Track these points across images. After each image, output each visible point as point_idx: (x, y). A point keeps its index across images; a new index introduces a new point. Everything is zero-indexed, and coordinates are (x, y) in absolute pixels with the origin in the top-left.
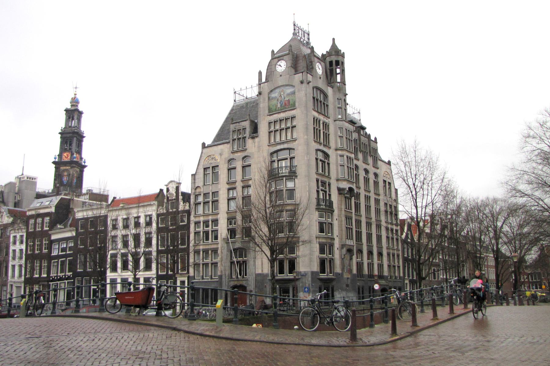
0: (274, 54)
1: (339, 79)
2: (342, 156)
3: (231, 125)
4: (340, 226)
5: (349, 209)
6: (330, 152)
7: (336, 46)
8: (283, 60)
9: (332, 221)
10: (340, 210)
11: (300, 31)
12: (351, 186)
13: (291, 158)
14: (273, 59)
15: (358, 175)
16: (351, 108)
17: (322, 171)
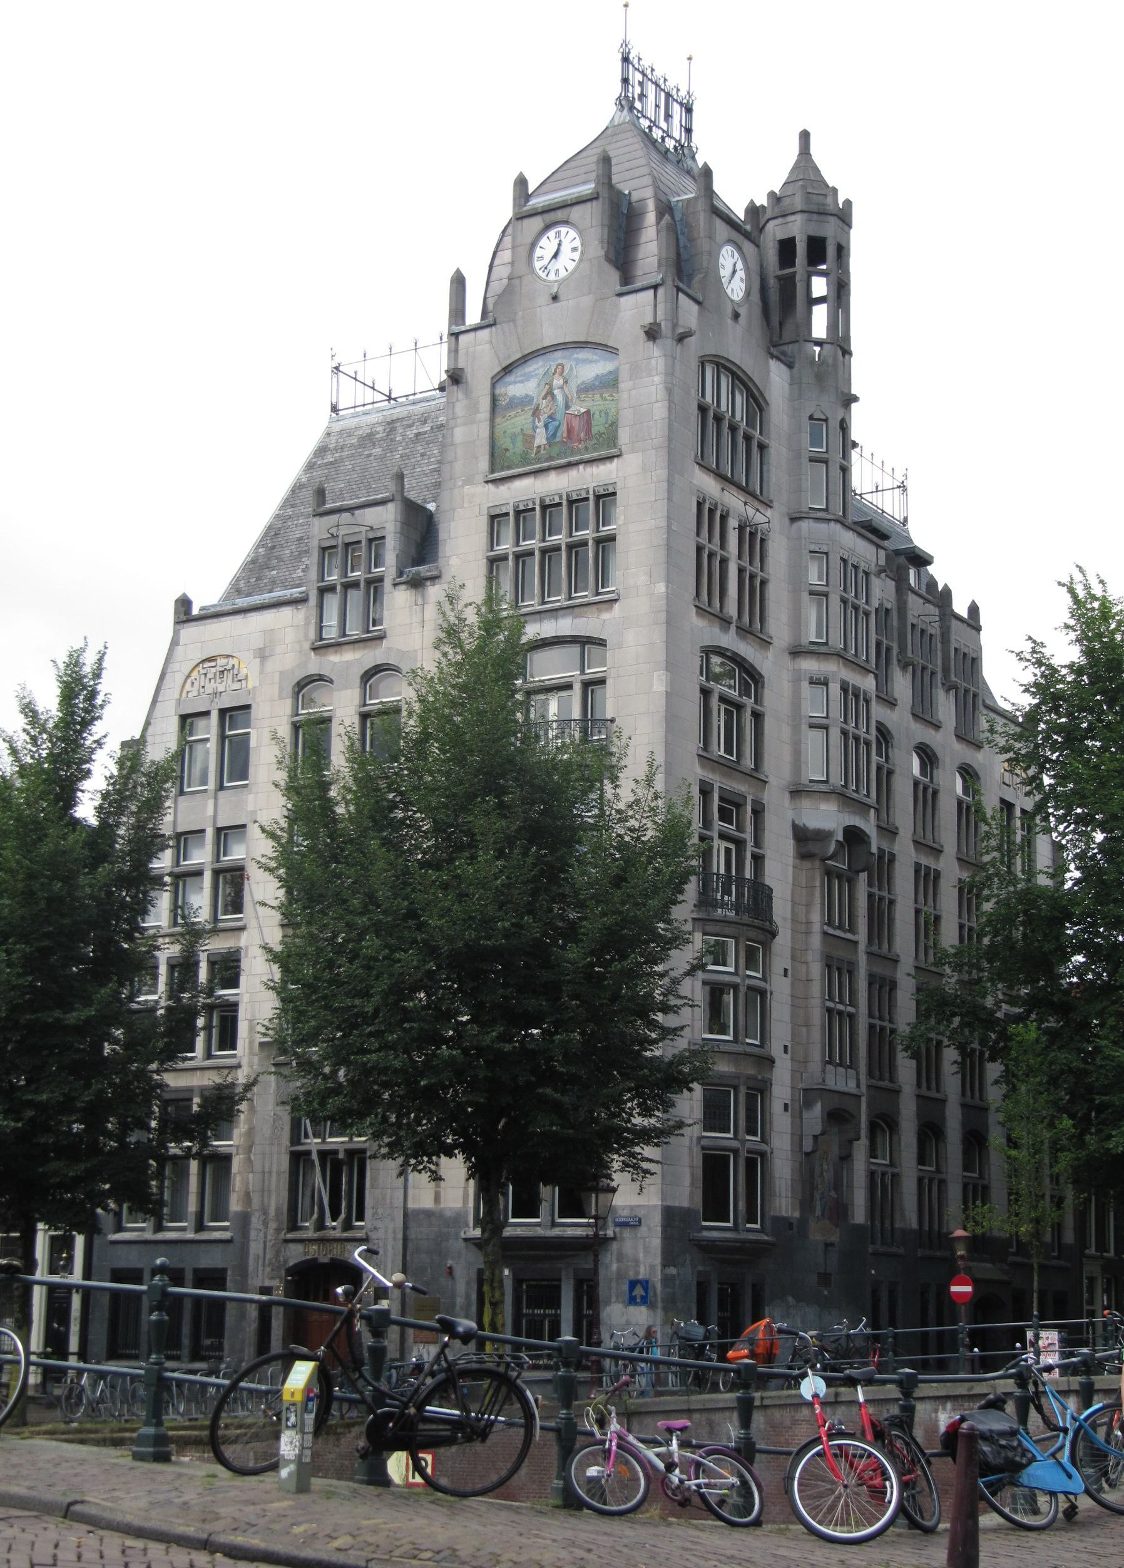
0: (528, 197)
1: (819, 327)
2: (820, 682)
3: (317, 521)
4: (798, 1001)
5: (840, 927)
6: (766, 662)
7: (816, 170)
8: (566, 222)
9: (764, 979)
10: (801, 928)
11: (651, 89)
12: (856, 821)
13: (586, 685)
14: (520, 217)
15: (890, 773)
16: (867, 465)
17: (728, 750)
